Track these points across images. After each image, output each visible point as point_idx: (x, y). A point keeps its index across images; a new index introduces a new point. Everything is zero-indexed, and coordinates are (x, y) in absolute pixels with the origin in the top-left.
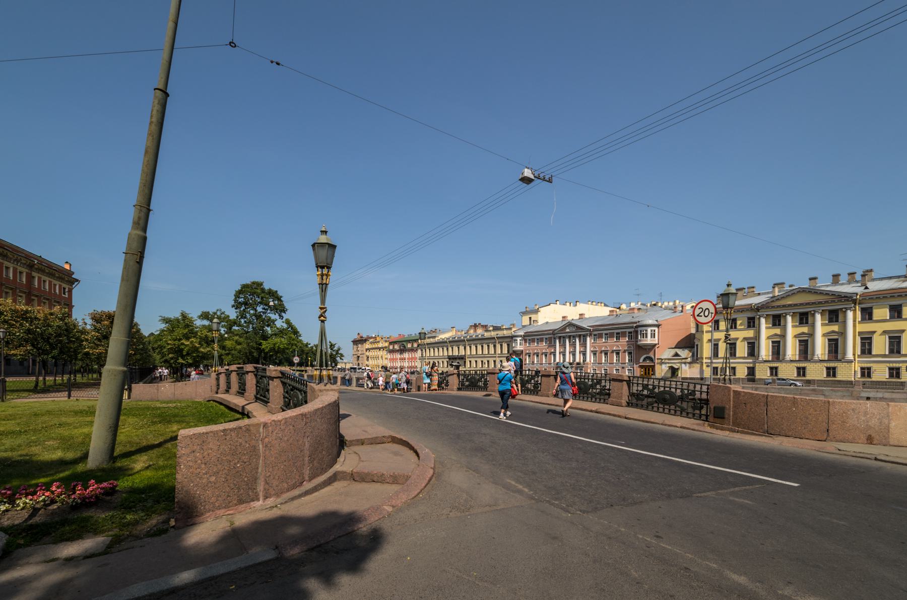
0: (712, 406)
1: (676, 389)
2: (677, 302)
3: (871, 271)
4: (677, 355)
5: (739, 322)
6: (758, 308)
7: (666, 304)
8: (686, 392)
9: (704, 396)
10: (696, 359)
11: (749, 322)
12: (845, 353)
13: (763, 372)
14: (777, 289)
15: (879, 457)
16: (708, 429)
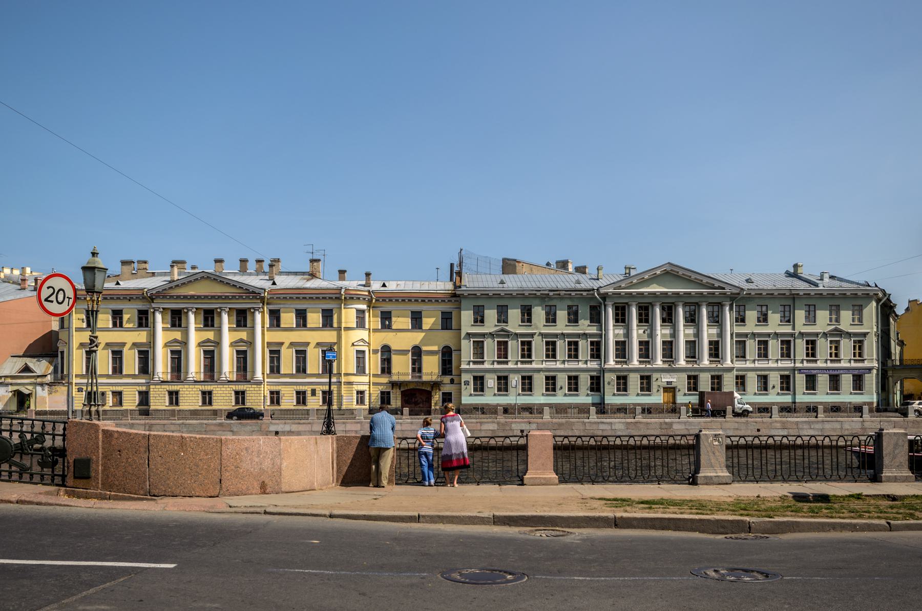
0: (71, 458)
1: (11, 432)
2: (28, 270)
3: (278, 261)
4: (26, 369)
5: (126, 317)
6: (151, 297)
7: (7, 271)
8: (28, 436)
9: (59, 442)
10: (61, 377)
11: (140, 319)
12: (254, 372)
13: (159, 401)
14: (176, 270)
15: (268, 510)
16: (64, 499)
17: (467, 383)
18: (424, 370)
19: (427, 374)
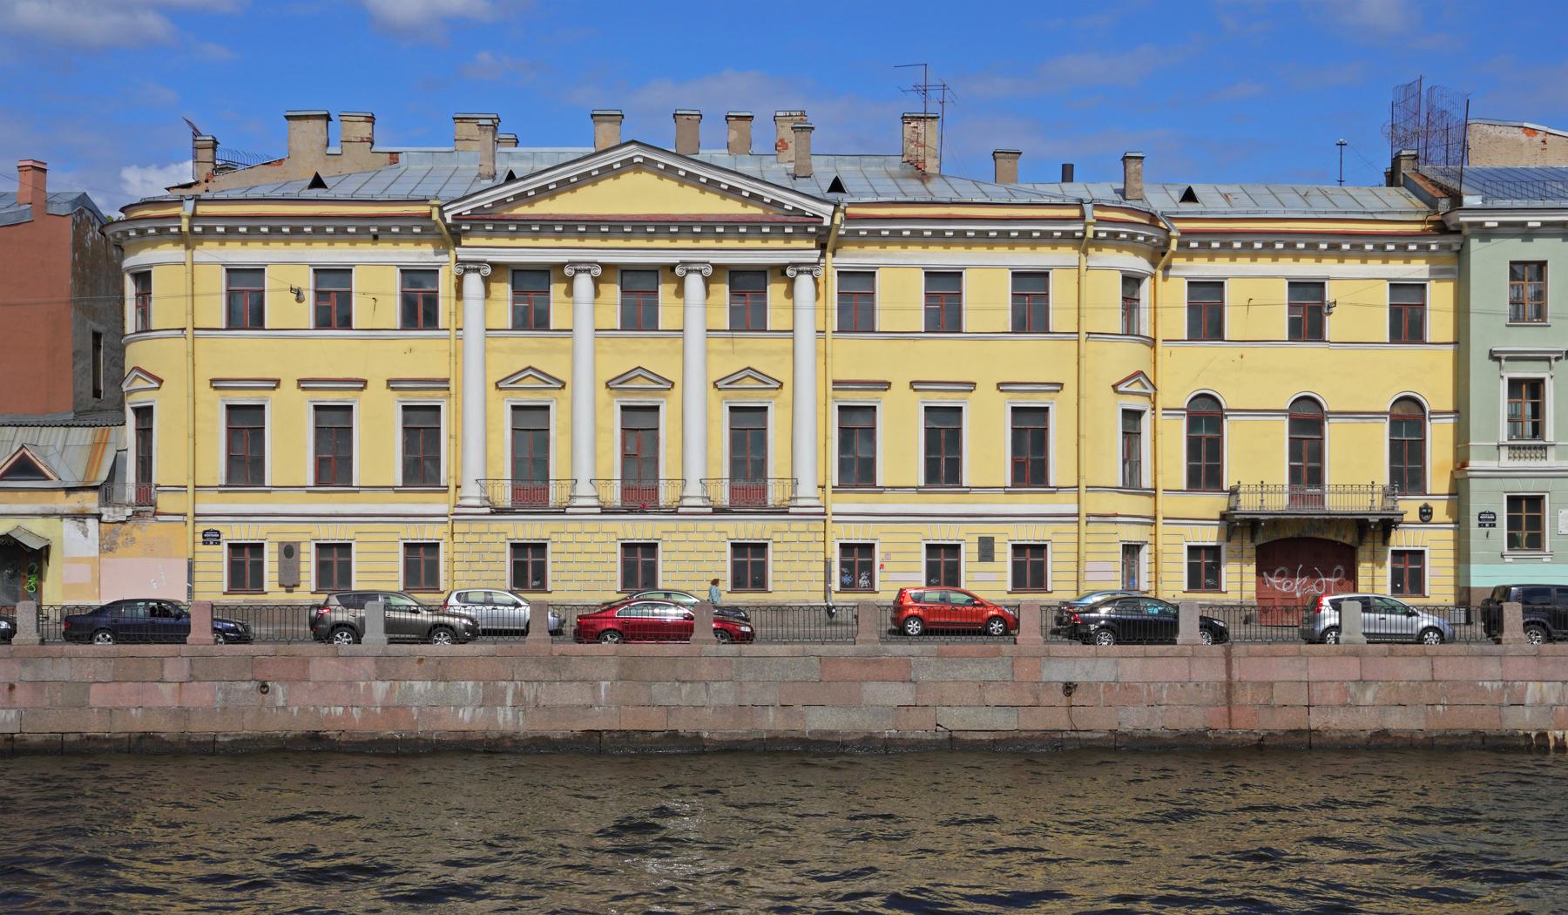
17: (1487, 520)
18: (1330, 477)
19: (1342, 490)
